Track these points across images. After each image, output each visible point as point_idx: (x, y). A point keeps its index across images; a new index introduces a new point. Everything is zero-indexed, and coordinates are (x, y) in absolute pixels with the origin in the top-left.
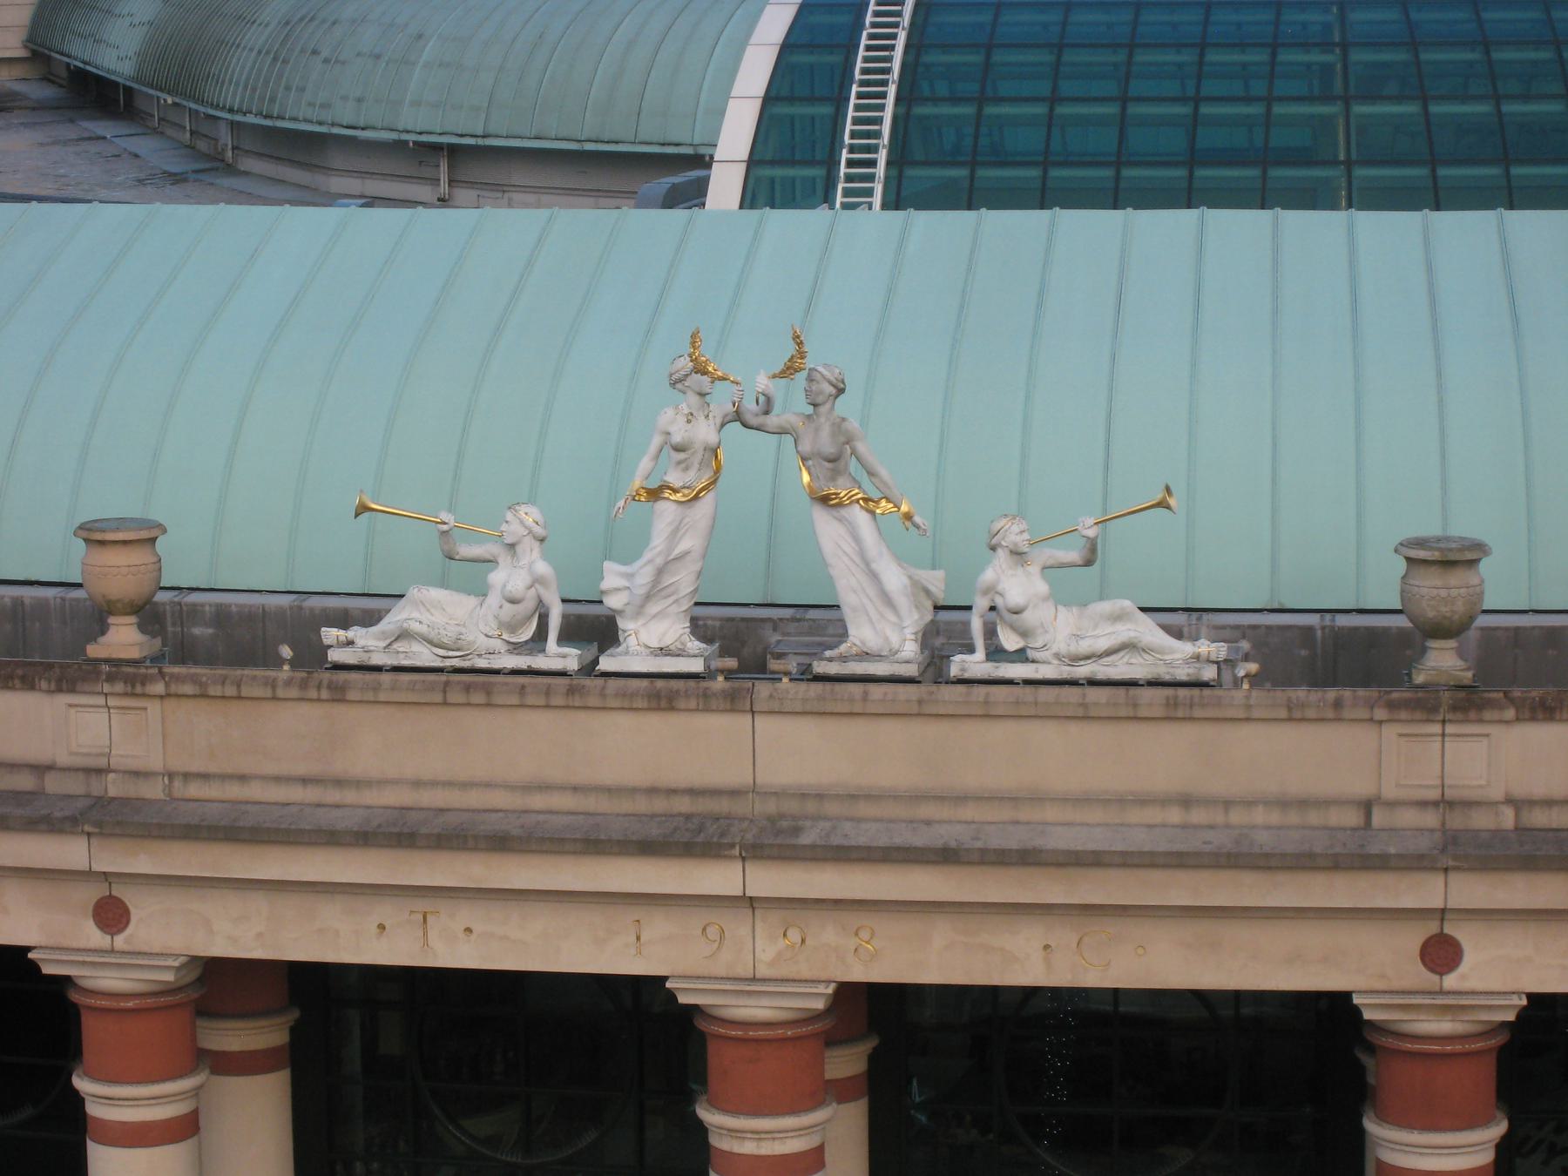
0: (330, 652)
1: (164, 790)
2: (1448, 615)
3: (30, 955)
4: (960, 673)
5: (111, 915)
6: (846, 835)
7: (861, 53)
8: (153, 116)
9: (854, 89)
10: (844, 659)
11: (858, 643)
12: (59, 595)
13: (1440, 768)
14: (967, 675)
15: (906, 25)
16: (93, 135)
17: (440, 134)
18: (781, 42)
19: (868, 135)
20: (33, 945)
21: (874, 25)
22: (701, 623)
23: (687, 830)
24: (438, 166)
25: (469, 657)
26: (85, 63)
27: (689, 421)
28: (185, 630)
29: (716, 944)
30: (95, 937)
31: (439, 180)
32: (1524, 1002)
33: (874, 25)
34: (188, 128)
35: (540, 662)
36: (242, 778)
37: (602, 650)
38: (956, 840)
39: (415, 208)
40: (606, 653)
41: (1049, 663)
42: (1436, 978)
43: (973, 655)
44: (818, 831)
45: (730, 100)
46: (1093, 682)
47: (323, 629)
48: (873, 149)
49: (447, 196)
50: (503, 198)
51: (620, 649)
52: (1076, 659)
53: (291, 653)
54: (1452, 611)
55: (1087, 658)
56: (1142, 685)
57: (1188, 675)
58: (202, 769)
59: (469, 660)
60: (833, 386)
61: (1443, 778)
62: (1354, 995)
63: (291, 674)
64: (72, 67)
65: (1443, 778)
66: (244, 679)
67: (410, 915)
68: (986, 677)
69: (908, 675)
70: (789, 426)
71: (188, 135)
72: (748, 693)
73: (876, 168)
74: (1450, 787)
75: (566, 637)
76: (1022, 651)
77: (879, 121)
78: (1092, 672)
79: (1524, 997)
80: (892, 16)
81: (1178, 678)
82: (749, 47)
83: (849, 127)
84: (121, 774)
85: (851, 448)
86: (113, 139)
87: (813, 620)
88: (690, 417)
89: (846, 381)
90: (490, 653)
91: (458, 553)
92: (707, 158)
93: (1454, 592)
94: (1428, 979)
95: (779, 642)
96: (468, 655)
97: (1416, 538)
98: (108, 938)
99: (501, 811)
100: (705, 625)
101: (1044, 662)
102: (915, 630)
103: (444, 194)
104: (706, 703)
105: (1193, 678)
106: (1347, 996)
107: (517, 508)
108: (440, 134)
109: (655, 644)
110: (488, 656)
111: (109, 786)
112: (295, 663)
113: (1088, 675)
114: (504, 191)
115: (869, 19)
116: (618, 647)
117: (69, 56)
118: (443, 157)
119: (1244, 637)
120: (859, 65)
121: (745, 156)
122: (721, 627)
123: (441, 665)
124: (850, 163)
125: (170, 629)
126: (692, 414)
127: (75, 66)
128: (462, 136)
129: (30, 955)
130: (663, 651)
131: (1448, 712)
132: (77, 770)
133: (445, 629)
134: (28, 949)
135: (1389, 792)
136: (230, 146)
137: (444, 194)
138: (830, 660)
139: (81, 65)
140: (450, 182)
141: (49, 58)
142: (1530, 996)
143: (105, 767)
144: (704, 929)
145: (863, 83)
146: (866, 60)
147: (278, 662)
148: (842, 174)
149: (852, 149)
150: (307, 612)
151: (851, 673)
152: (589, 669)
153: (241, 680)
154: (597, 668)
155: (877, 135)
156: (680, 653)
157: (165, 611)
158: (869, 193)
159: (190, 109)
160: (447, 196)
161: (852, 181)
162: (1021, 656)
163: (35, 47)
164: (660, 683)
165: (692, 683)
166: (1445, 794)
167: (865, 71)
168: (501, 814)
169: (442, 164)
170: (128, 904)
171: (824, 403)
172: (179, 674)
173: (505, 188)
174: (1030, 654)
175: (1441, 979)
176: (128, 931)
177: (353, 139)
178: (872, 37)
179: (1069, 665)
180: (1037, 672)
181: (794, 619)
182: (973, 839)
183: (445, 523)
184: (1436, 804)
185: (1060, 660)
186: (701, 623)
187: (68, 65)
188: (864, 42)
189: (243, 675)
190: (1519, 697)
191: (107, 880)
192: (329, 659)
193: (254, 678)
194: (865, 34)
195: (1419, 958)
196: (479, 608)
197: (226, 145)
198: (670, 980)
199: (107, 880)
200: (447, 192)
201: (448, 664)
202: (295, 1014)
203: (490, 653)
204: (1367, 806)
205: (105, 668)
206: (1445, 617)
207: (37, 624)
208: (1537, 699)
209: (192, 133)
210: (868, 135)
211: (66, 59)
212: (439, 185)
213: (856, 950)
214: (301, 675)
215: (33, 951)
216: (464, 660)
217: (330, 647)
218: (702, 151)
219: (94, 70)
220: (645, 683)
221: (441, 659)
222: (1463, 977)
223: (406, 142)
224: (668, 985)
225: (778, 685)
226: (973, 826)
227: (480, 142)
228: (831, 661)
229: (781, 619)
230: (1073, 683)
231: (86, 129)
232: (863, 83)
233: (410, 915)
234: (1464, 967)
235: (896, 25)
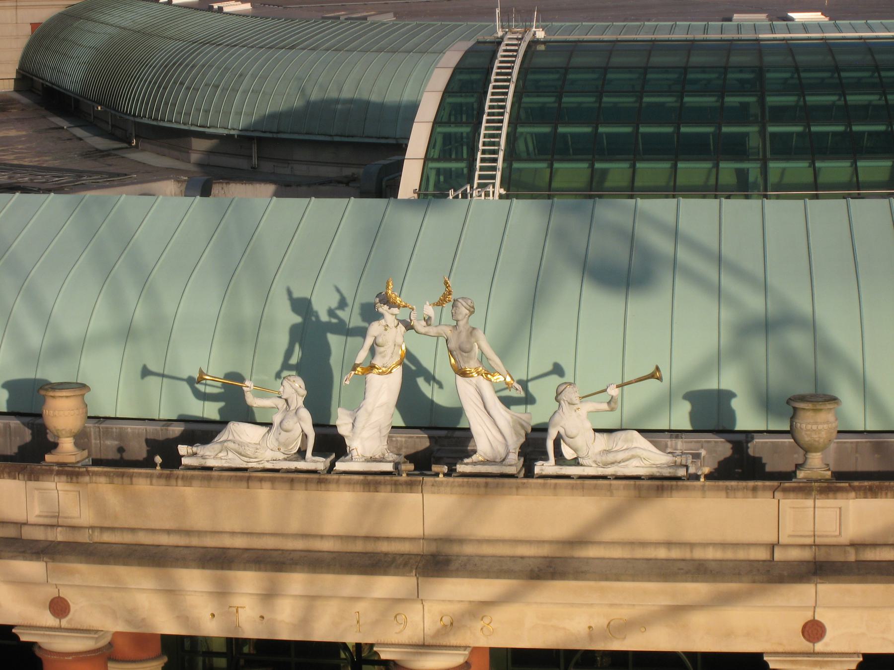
0: (183, 459)
1: (89, 537)
2: (817, 439)
3: (14, 631)
4: (540, 472)
5: (59, 607)
6: (476, 565)
7: (489, 97)
8: (90, 115)
9: (485, 117)
10: (475, 463)
11: (483, 455)
12: (31, 422)
13: (813, 527)
14: (544, 473)
15: (514, 80)
16: (56, 126)
17: (252, 131)
18: (454, 66)
19: (493, 144)
20: (15, 624)
21: (496, 81)
22: (394, 439)
23: (386, 561)
24: (252, 149)
25: (262, 462)
26: (53, 84)
27: (386, 330)
28: (102, 442)
29: (403, 625)
30: (49, 620)
31: (252, 157)
32: (861, 659)
33: (496, 81)
34: (110, 123)
35: (301, 465)
36: (133, 530)
37: (337, 458)
38: (538, 567)
39: (180, 416)
40: (339, 460)
41: (591, 466)
42: (811, 645)
43: (548, 462)
44: (460, 562)
45: (425, 93)
46: (618, 478)
47: (179, 446)
48: (495, 152)
49: (256, 166)
50: (288, 167)
51: (347, 458)
52: (606, 465)
53: (161, 460)
54: (819, 437)
55: (613, 463)
56: (644, 479)
57: (670, 473)
58: (111, 525)
59: (262, 464)
60: (468, 310)
61: (814, 531)
62: (764, 655)
63: (161, 472)
64: (45, 86)
65: (814, 531)
66: (134, 474)
67: (229, 608)
68: (555, 474)
69: (511, 473)
70: (442, 332)
71: (110, 127)
72: (419, 484)
73: (497, 163)
74: (819, 536)
75: (317, 451)
76: (576, 459)
77: (499, 136)
78: (615, 471)
79: (861, 656)
80: (504, 89)
81: (664, 474)
82: (436, 70)
83: (482, 139)
84: (65, 528)
85: (477, 344)
86: (68, 129)
87: (458, 438)
88: (386, 328)
89: (475, 307)
90: (274, 460)
91: (255, 403)
92: (404, 146)
93: (820, 427)
94: (806, 646)
95: (438, 450)
96: (261, 461)
97: (799, 395)
98: (58, 620)
99: (279, 550)
100: (397, 440)
101: (588, 466)
102: (514, 447)
103: (255, 164)
104: (397, 487)
105: (672, 475)
106: (759, 656)
107: (289, 378)
108: (252, 131)
109: (368, 455)
110: (272, 462)
111: (58, 535)
112: (163, 466)
113: (613, 473)
114: (289, 163)
115: (493, 77)
116: (345, 457)
117: (43, 79)
118: (255, 143)
119: (702, 447)
120: (488, 103)
121: (423, 156)
122: (406, 442)
123: (246, 466)
124: (483, 160)
125: (93, 441)
126: (388, 326)
127: (46, 85)
128: (265, 132)
129: (14, 631)
130: (373, 460)
131: (817, 495)
132: (40, 525)
133: (248, 446)
134: (12, 627)
135: (784, 540)
136: (134, 135)
137: (255, 164)
138: (467, 464)
139: (50, 85)
140: (258, 157)
141: (32, 79)
142: (865, 656)
143: (55, 524)
144: (396, 617)
145: (489, 114)
146: (492, 100)
147: (154, 465)
148: (478, 167)
149: (484, 152)
150: (171, 432)
151: (478, 471)
152: (331, 469)
153: (133, 475)
154: (334, 469)
155: (498, 144)
156: (382, 460)
157: (90, 431)
158: (493, 177)
159: (111, 113)
160: (256, 166)
161: (498, 134)
162: (576, 462)
163: (24, 73)
164: (370, 478)
165: (388, 478)
166: (816, 540)
167: (491, 107)
168: (280, 552)
169: (254, 147)
170: (69, 601)
171: (462, 320)
172: (97, 471)
173: (290, 162)
174: (581, 461)
175: (814, 646)
176: (70, 616)
177: (204, 133)
178: (495, 87)
179: (602, 467)
180: (584, 471)
181: (446, 437)
182: (548, 567)
183: (248, 387)
184: (810, 546)
185: (597, 464)
186: (394, 439)
187: (43, 84)
188: (490, 90)
189: (133, 472)
190: (857, 486)
191: (57, 588)
192: (183, 463)
193: (140, 474)
194: (491, 86)
195: (801, 633)
196: (267, 434)
197: (131, 134)
198: (376, 646)
199: (57, 588)
200: (256, 163)
201: (250, 466)
202: (165, 659)
203: (274, 460)
204: (772, 547)
205: (56, 468)
206: (815, 441)
207: (18, 438)
208: (868, 487)
209: (113, 126)
210: (493, 144)
211: (41, 81)
212: (252, 159)
213: (482, 629)
214: (167, 472)
215: (16, 628)
216: (259, 464)
217: (183, 456)
218: (401, 141)
219: (57, 88)
220: (361, 477)
221: (246, 463)
222: (826, 645)
223: (233, 135)
224: (375, 649)
225: (437, 479)
226: (548, 560)
227: (275, 136)
228: (467, 465)
229: (439, 437)
230: (604, 477)
231: (53, 122)
232: (489, 114)
233: (229, 608)
234: (826, 639)
235: (509, 81)
